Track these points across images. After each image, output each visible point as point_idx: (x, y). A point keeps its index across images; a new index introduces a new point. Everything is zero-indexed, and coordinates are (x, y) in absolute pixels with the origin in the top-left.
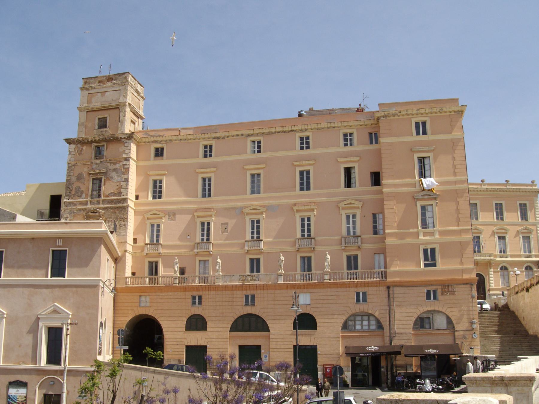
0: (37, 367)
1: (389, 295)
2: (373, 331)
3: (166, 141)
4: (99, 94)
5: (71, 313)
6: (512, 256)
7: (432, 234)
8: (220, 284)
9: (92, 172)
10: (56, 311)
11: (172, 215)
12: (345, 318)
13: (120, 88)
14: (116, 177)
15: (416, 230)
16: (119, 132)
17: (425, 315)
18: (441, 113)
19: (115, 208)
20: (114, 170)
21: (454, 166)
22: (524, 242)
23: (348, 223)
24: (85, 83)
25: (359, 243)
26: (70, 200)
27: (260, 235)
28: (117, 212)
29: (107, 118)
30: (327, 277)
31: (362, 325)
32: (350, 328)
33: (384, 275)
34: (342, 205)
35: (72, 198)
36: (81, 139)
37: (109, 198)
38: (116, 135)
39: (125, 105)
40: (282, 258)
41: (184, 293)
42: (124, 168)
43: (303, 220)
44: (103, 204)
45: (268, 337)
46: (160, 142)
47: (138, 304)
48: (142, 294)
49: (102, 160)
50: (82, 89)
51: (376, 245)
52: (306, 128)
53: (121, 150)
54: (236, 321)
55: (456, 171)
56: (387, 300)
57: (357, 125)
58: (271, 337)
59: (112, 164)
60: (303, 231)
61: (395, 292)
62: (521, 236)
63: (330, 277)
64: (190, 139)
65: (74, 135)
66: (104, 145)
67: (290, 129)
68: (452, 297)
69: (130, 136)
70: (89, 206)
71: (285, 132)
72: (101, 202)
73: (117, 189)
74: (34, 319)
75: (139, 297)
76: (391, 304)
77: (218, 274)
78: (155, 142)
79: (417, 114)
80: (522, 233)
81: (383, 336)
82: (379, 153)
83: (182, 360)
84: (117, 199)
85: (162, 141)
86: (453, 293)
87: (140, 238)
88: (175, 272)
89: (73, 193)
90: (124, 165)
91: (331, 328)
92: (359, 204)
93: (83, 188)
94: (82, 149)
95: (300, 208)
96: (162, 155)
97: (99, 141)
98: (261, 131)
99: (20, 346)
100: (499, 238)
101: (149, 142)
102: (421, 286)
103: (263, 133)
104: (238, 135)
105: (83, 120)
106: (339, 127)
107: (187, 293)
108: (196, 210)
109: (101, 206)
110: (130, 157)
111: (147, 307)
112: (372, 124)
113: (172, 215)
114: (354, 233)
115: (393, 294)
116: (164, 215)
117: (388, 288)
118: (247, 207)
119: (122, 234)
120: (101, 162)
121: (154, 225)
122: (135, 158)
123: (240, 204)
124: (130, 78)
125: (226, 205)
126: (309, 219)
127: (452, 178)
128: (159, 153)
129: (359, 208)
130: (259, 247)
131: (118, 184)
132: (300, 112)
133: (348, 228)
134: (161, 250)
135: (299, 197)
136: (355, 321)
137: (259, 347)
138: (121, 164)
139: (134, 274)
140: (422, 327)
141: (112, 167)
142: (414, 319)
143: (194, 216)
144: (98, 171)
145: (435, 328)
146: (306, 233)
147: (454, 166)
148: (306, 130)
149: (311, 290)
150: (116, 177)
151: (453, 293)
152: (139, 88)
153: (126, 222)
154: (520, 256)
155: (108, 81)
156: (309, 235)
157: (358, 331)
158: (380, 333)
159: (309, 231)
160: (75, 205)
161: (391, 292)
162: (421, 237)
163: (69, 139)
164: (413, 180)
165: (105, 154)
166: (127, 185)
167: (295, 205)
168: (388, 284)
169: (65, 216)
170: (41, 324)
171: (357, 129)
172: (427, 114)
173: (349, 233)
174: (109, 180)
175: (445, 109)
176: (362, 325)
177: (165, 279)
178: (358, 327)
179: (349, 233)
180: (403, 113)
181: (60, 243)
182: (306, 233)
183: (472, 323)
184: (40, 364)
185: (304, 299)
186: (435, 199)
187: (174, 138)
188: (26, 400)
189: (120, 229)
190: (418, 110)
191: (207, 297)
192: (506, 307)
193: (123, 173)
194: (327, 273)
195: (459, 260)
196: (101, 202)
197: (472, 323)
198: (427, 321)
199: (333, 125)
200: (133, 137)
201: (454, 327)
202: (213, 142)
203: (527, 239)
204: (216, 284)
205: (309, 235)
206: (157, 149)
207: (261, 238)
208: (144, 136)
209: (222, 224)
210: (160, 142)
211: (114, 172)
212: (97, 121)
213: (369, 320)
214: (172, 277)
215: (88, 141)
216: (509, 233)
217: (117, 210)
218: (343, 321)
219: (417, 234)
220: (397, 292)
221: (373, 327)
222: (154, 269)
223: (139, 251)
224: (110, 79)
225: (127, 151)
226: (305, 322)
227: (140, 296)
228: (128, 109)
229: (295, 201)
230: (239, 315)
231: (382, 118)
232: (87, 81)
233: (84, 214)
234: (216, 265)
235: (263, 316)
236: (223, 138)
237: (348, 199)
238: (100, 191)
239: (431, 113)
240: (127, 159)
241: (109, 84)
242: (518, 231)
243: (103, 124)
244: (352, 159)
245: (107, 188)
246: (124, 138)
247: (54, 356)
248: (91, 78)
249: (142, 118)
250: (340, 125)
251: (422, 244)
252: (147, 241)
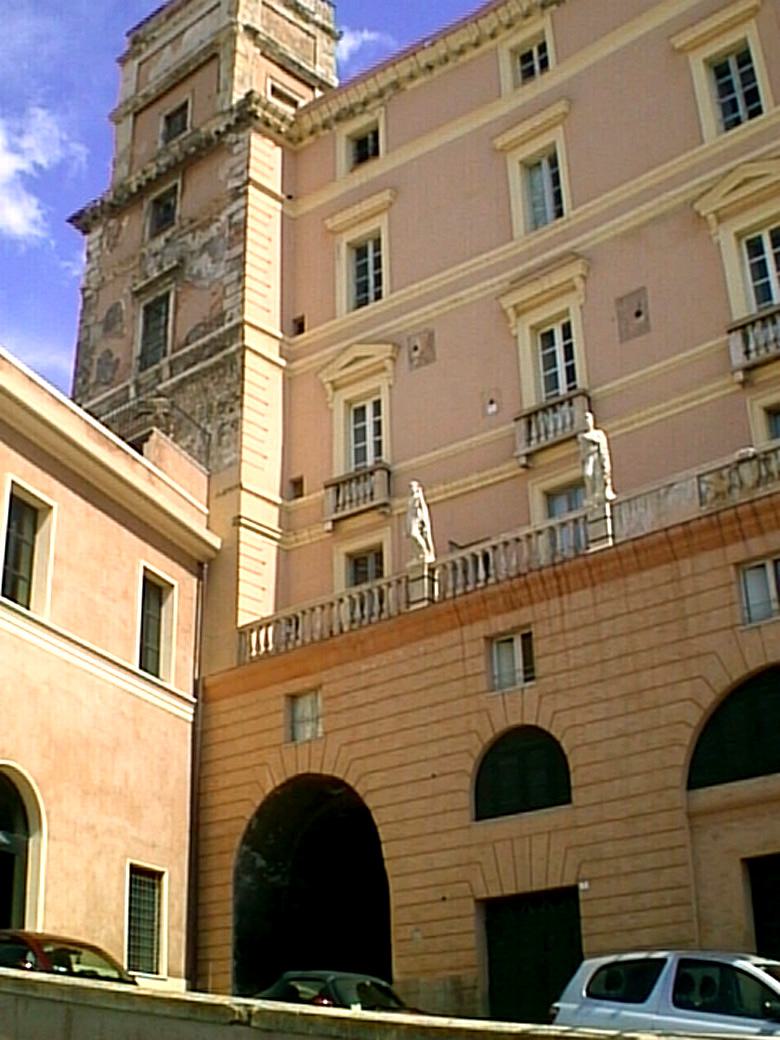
3: (381, 94)
28: (211, 385)
36: (109, 198)
37: (192, 346)
39: (233, 35)
41: (455, 634)
47: (280, 735)
59: (198, 233)
64: (461, 52)
75: (282, 703)
94: (120, 227)
97: (161, 177)
101: (326, 125)
119: (227, 461)
120: (167, 240)
126: (744, 58)
153: (237, 413)
166: (241, 278)
174: (192, 286)
189: (219, 443)
191: (557, 623)
200: (253, 114)
204: (594, 548)
227: (293, 698)
228: (243, 44)
245: (183, 318)
246: (229, 128)
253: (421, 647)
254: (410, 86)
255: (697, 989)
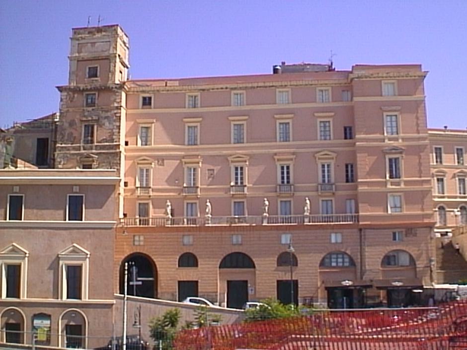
0: (59, 301)
1: (361, 236)
2: (347, 267)
3: (154, 91)
4: (89, 45)
5: (89, 253)
6: (449, 197)
7: (398, 184)
8: (210, 225)
9: (84, 119)
10: (75, 251)
11: (161, 160)
12: (322, 256)
13: (110, 40)
14: (107, 124)
15: (384, 180)
16: (110, 82)
17: (391, 254)
18: (407, 77)
19: (107, 153)
20: (106, 118)
21: (418, 125)
22: (460, 184)
23: (323, 171)
24: (75, 33)
25: (334, 189)
26: (63, 145)
27: (244, 181)
28: (110, 157)
29: (97, 67)
30: (306, 220)
31: (337, 262)
32: (327, 265)
33: (357, 218)
34: (317, 155)
35: (65, 144)
38: (108, 85)
39: (116, 57)
40: (267, 203)
41: (176, 233)
42: (116, 116)
43: (282, 168)
44: (96, 150)
45: (255, 274)
46: (148, 92)
47: (132, 243)
48: (136, 234)
49: (94, 108)
50: (71, 39)
51: (349, 192)
52: (286, 84)
53: (112, 99)
54: (225, 258)
55: (419, 128)
56: (359, 241)
57: (332, 84)
58: (257, 272)
59: (104, 112)
60: (283, 178)
61: (367, 234)
62: (457, 179)
63: (310, 220)
65: (65, 83)
66: (95, 94)
67: (271, 85)
68: (414, 238)
69: (121, 86)
70: (82, 151)
71: (266, 87)
72: (94, 148)
73: (110, 136)
74: (54, 257)
76: (363, 244)
77: (208, 217)
78: (143, 92)
79: (386, 77)
80: (458, 176)
81: (355, 272)
82: (352, 109)
83: (175, 294)
84: (110, 145)
85: (150, 91)
86: (415, 235)
87: (130, 180)
88: (166, 213)
89: (66, 138)
90: (116, 113)
91: (310, 265)
92: (334, 155)
93: (76, 134)
94: (74, 96)
95: (281, 157)
96: (150, 104)
97: (91, 90)
98: (244, 85)
99: (42, 283)
100: (438, 180)
102: (388, 229)
103: (246, 87)
104: (222, 88)
105: (74, 69)
106: (315, 85)
107: (179, 233)
108: (184, 157)
109: (94, 151)
110: (121, 106)
111: (141, 245)
112: (346, 83)
113: (161, 160)
114: (329, 181)
115: (365, 235)
116: (153, 160)
117: (361, 230)
118: (231, 155)
121: (143, 170)
122: (125, 107)
123: (225, 152)
124: (119, 31)
125: (211, 153)
126: (288, 168)
127: (416, 135)
128: (147, 102)
129: (333, 158)
130: (244, 191)
131: (110, 131)
132: (276, 66)
133: (324, 176)
134: (151, 194)
135: (280, 147)
136: (331, 258)
137: (246, 282)
138: (113, 112)
139: (125, 215)
140: (389, 264)
141: (104, 115)
142: (382, 257)
143: (181, 162)
144: (90, 118)
145: (400, 265)
146: (285, 180)
147: (418, 125)
148: (286, 86)
149: (292, 232)
150: (107, 124)
151: (415, 235)
152: (126, 39)
154: (456, 197)
155: (98, 32)
156: (288, 182)
157: (334, 267)
158: (353, 269)
159: (288, 178)
160: (69, 150)
161: (362, 234)
162: (389, 186)
163: (62, 87)
164: (382, 136)
165: (96, 102)
166: (119, 132)
167: (276, 154)
168: (360, 227)
169: (59, 160)
170: (61, 262)
171: (332, 87)
172: (395, 77)
173: (324, 181)
175: (411, 74)
176: (337, 262)
177: (158, 220)
178: (334, 264)
179: (324, 181)
180: (375, 76)
181: (76, 189)
182: (285, 180)
183: (431, 261)
184: (62, 298)
185: (286, 239)
186: (401, 153)
187: (162, 89)
188: (50, 330)
190: (387, 73)
192: (450, 245)
193: (115, 121)
194: (307, 216)
195: (420, 206)
196: (94, 148)
197: (431, 261)
198: (392, 259)
199: (310, 83)
200: (123, 87)
201: (415, 264)
202: (198, 94)
203: (462, 181)
204: (207, 225)
205: (288, 182)
206: (144, 99)
207: (244, 184)
208: (133, 86)
209: (209, 170)
210: (148, 92)
211: (106, 120)
212: (87, 70)
213: (343, 258)
214: (164, 218)
215: (80, 90)
216: (447, 175)
217: (111, 157)
218: (321, 259)
219: (385, 183)
220: (369, 233)
221: (347, 264)
222: (143, 211)
223: (129, 194)
224: (99, 30)
225: (118, 100)
226: (287, 260)
228: (118, 60)
229: (276, 151)
230: (228, 253)
231: (356, 79)
232: (76, 31)
233: (78, 158)
234: (206, 209)
235: (249, 254)
236: (208, 90)
237: (324, 150)
238: (92, 136)
239: (399, 77)
240: (119, 108)
241: (99, 35)
242: (454, 174)
243: (93, 73)
244: (327, 114)
247: (75, 290)
248: (81, 29)
249: (127, 68)
250: (316, 82)
251: (390, 192)
252: (138, 185)
253: (169, 234)
254: (162, 92)
255: (115, 339)
